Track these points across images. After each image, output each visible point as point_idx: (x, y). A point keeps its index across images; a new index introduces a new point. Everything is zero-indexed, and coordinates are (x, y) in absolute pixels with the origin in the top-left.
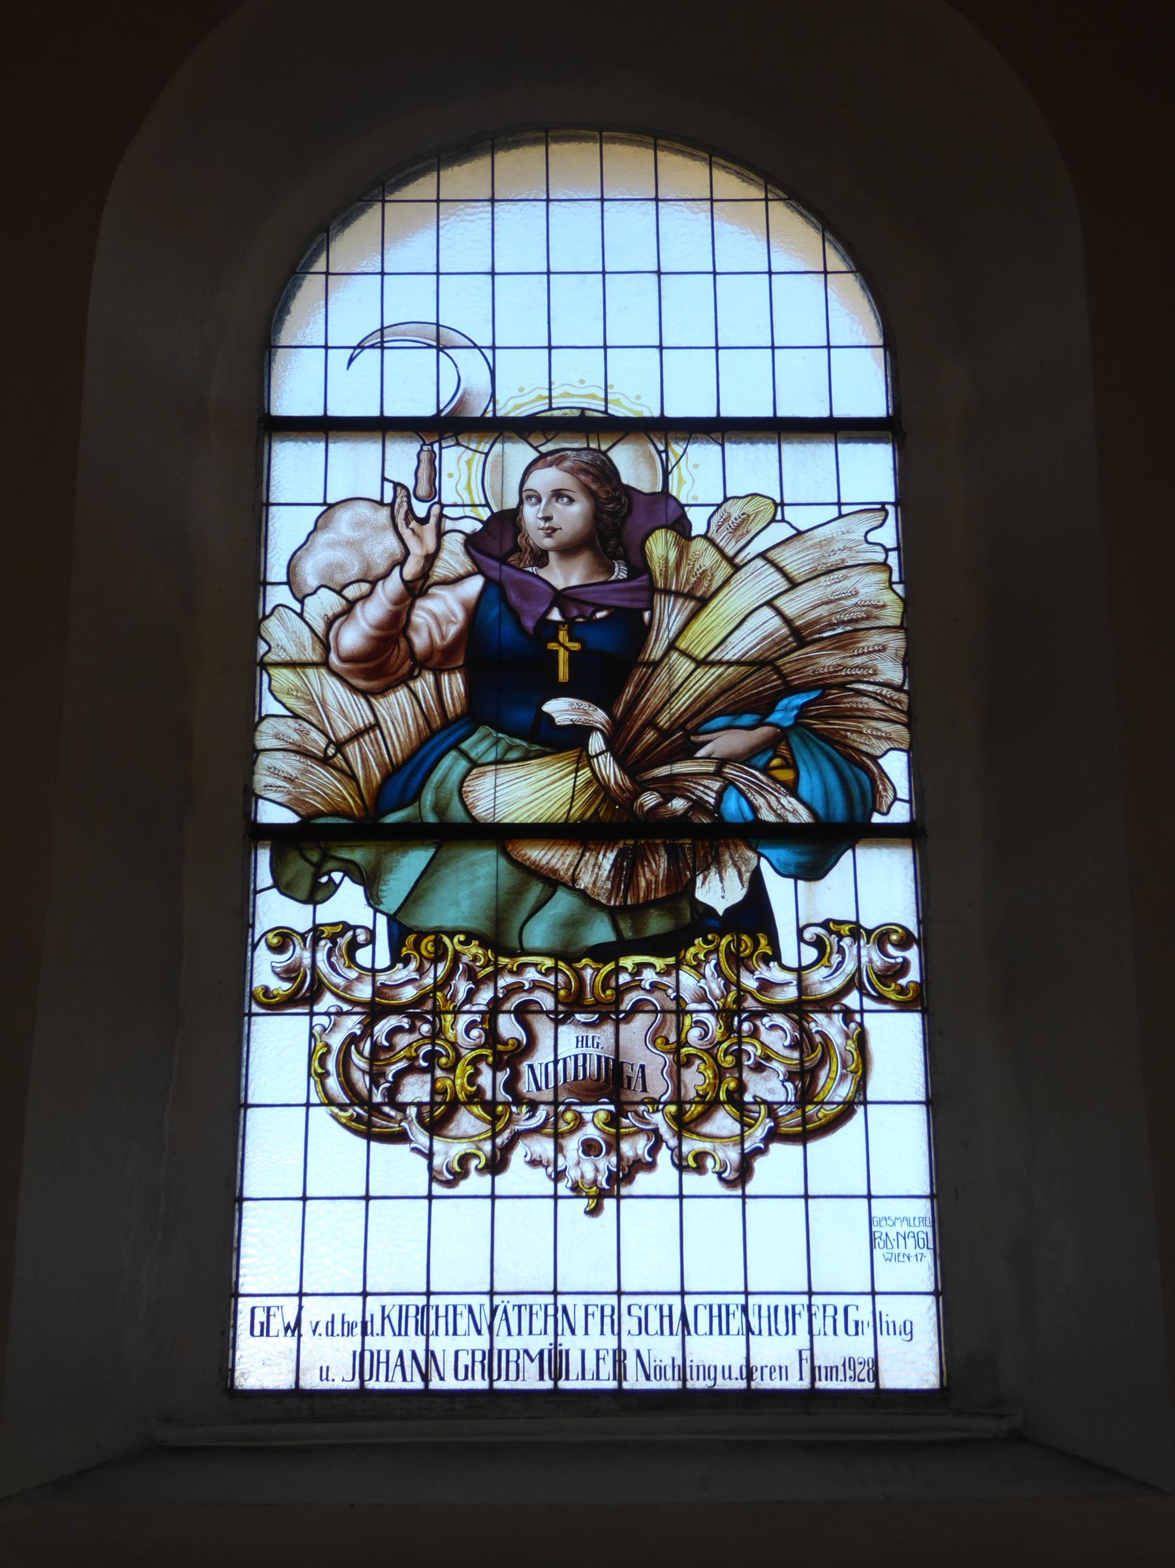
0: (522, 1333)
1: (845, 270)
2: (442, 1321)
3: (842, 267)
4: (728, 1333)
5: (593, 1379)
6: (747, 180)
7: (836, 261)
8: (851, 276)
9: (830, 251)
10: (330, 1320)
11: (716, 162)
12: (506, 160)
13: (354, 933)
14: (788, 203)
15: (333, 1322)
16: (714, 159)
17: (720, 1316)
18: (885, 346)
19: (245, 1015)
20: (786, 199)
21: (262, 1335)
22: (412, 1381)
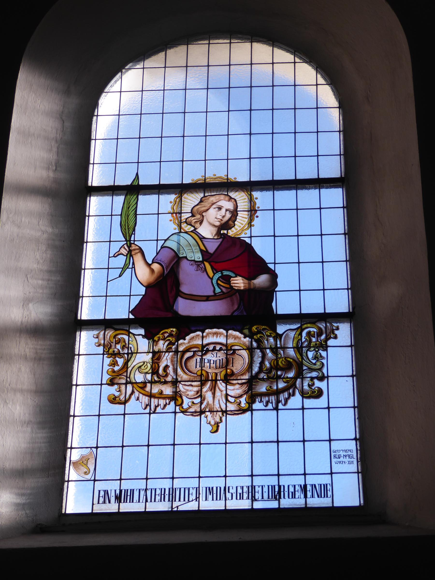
0: (267, 486)
1: (326, 84)
2: (129, 497)
3: (324, 82)
4: (268, 486)
5: (310, 498)
6: (299, 57)
7: (321, 80)
8: (327, 86)
9: (319, 76)
10: (198, 486)
11: (297, 55)
12: (171, 52)
13: (279, 348)
14: (310, 64)
15: (199, 487)
16: (296, 53)
17: (130, 496)
18: (339, 108)
19: (355, 376)
20: (308, 62)
21: (124, 502)
22: (300, 498)
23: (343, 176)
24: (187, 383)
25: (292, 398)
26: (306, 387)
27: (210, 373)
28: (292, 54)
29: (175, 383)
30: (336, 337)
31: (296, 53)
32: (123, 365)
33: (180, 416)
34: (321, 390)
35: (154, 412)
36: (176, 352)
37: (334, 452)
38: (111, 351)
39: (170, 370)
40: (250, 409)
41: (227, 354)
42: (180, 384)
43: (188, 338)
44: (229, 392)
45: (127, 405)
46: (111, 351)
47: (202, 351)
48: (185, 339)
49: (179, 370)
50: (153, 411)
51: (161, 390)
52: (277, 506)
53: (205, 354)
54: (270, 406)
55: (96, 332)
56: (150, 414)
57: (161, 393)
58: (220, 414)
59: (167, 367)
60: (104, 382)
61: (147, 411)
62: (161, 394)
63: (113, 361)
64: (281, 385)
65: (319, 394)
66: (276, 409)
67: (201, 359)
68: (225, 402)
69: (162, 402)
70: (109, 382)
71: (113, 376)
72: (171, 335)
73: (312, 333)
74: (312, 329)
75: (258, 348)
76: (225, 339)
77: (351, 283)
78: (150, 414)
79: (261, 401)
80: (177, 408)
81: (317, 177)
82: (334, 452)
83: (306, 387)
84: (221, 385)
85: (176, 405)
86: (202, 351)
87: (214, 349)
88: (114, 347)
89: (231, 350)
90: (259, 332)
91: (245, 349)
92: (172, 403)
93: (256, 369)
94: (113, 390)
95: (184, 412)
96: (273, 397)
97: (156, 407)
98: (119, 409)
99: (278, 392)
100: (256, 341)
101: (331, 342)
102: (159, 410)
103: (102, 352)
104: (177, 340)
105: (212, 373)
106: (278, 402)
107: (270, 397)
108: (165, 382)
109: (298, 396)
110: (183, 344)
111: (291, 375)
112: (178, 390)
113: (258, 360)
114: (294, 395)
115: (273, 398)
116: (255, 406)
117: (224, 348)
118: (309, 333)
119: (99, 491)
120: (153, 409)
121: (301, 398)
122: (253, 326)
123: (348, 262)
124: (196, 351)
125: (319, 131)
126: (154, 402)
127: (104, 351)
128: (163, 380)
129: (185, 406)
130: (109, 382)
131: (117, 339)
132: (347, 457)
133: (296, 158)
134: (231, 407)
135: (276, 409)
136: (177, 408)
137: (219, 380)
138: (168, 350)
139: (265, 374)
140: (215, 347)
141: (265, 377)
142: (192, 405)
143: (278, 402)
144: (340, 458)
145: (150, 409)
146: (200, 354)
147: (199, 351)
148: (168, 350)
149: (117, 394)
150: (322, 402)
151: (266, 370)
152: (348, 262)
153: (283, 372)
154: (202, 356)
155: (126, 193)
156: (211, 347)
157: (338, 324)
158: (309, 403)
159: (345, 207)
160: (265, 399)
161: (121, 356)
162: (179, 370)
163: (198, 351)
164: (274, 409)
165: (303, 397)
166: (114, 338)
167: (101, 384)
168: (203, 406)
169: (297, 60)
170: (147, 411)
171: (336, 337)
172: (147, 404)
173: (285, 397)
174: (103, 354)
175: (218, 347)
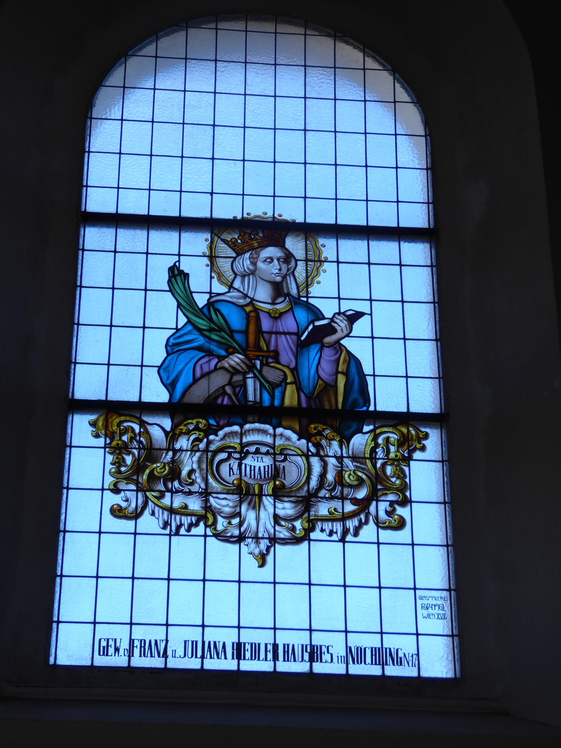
3: (407, 98)
16: (366, 50)
23: (431, 227)
24: (219, 496)
25: (365, 527)
26: (382, 515)
27: (251, 484)
28: (361, 52)
29: (206, 494)
30: (423, 449)
31: (366, 50)
32: (132, 463)
33: (212, 541)
34: (402, 519)
35: (177, 534)
36: (206, 450)
37: (420, 598)
38: (114, 443)
39: (197, 476)
40: (305, 537)
41: (275, 461)
42: (210, 497)
43: (221, 433)
44: (279, 512)
45: (138, 521)
46: (114, 443)
47: (241, 452)
48: (217, 436)
49: (211, 480)
50: (174, 532)
51: (184, 503)
52: (344, 672)
53: (244, 458)
54: (335, 537)
55: (93, 417)
56: (170, 535)
57: (186, 507)
58: (267, 541)
59: (192, 471)
60: (106, 486)
61: (167, 531)
62: (184, 511)
63: (117, 458)
64: (349, 507)
65: (401, 525)
66: (343, 540)
67: (240, 466)
68: (273, 524)
69: (186, 520)
70: (112, 487)
71: (117, 479)
72: (197, 428)
73: (392, 439)
74: (391, 435)
75: (317, 454)
76: (272, 438)
77: (445, 407)
78: (170, 535)
79: (322, 530)
80: (208, 530)
81: (396, 226)
82: (420, 598)
83: (382, 515)
84: (268, 501)
85: (206, 526)
86: (241, 452)
87: (257, 452)
88: (118, 438)
89: (281, 454)
90: (320, 433)
91: (301, 456)
92: (202, 524)
93: (314, 483)
94: (117, 499)
95: (217, 536)
96: (338, 524)
97: (179, 527)
98: (129, 525)
99: (344, 518)
100: (314, 445)
101: (417, 455)
102: (183, 531)
103: (103, 445)
104: (207, 436)
105: (254, 485)
106: (345, 532)
107: (335, 524)
108: (190, 493)
109: (372, 525)
110: (216, 440)
111: (361, 494)
112: (209, 505)
113: (317, 468)
114: (367, 522)
115: (338, 527)
116: (313, 536)
117: (271, 451)
118: (387, 439)
119: (100, 640)
120: (174, 528)
121: (376, 527)
122: (311, 424)
123: (441, 380)
124: (231, 452)
125: (393, 104)
126: (176, 520)
127: (105, 444)
128: (187, 490)
129: (220, 527)
130: (112, 487)
131: (122, 427)
132: (437, 607)
133: (369, 202)
134: (283, 533)
135: (343, 540)
136: (208, 530)
137: (266, 495)
138: (194, 450)
139: (328, 492)
140: (257, 449)
141: (327, 496)
142: (228, 526)
143: (345, 532)
144: (428, 609)
145: (171, 530)
146: (237, 456)
147: (236, 452)
148: (194, 450)
149: (124, 505)
150: (403, 535)
151: (329, 486)
152: (430, 205)
153: (350, 490)
154: (241, 459)
155: (184, 400)
156: (252, 449)
157: (428, 430)
158: (386, 535)
159: (441, 378)
160: (328, 526)
161: (127, 451)
162: (211, 480)
163: (234, 452)
164: (340, 541)
165: (378, 527)
166: (117, 427)
167: (103, 489)
168: (243, 529)
169: (371, 63)
170: (167, 531)
171: (423, 449)
172: (166, 520)
173: (354, 524)
174: (105, 448)
175: (264, 449)
